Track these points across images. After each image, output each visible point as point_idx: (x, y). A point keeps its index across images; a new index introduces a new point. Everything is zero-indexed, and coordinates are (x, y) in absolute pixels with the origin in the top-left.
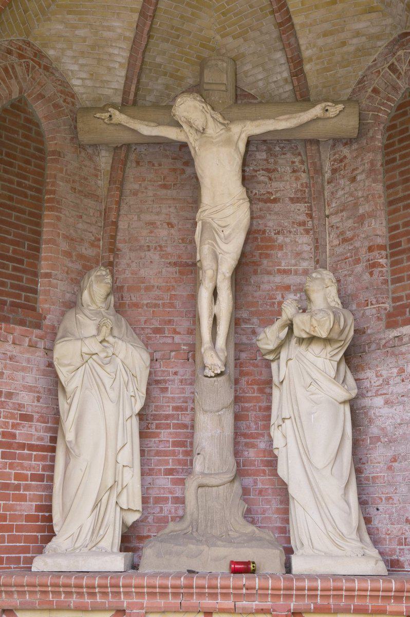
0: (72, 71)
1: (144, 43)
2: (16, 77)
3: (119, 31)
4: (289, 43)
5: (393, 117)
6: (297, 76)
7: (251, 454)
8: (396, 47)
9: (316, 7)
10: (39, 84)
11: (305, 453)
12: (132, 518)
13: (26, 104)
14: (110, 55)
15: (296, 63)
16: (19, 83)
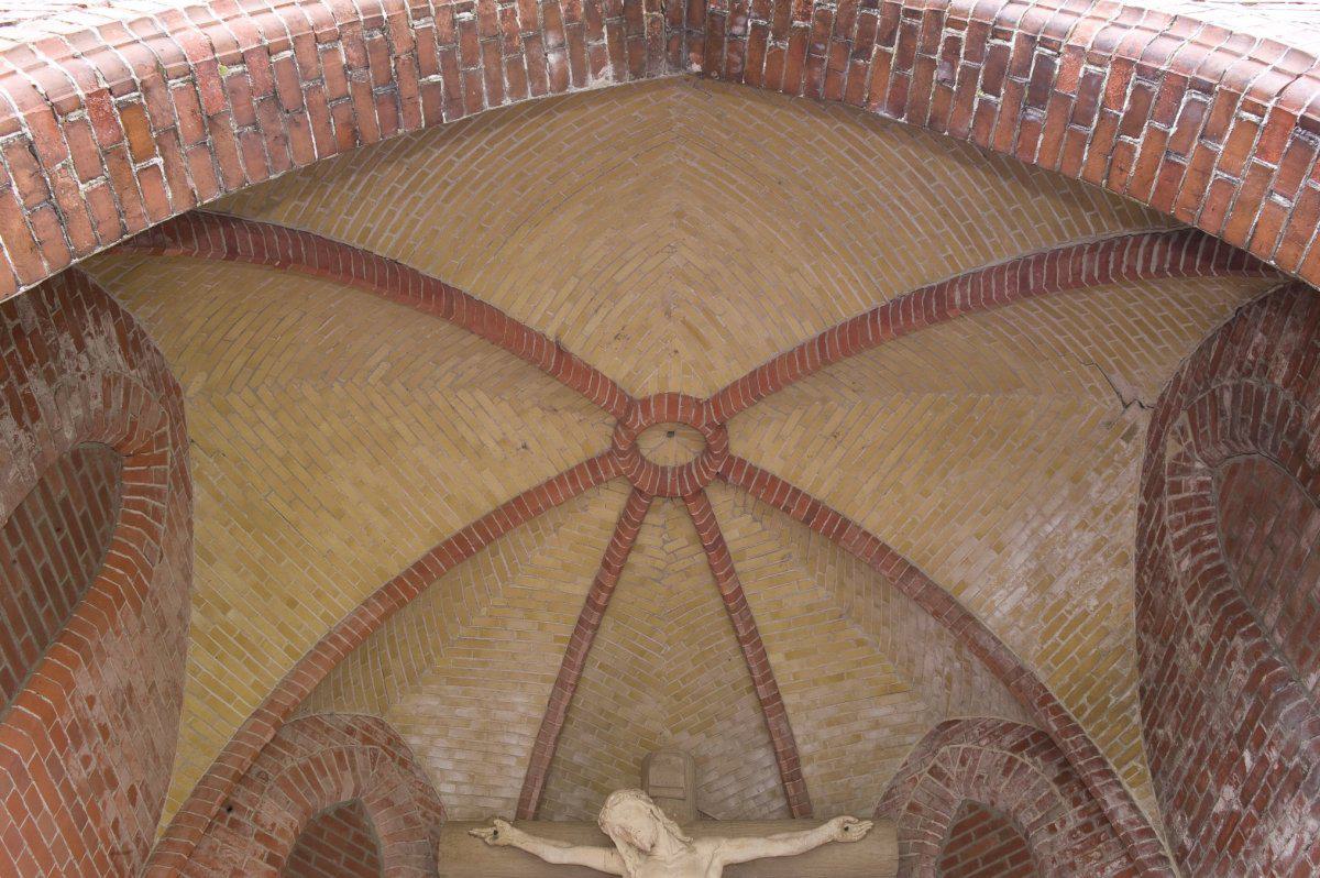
0: (442, 770)
1: (558, 725)
2: (354, 769)
3: (522, 709)
4: (779, 730)
5: (947, 847)
6: (792, 780)
8: (936, 743)
9: (815, 683)
10: (387, 783)
13: (361, 812)
14: (504, 745)
15: (789, 764)
16: (356, 778)
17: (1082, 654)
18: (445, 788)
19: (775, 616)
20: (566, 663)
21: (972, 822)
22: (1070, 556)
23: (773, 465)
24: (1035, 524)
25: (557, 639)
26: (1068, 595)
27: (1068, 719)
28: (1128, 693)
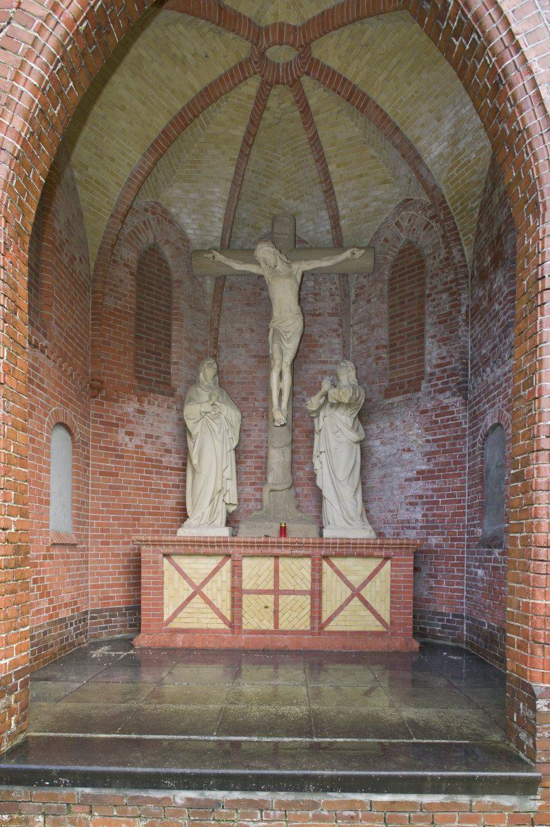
0: (187, 223)
2: (152, 228)
7: (300, 474)
10: (166, 233)
11: (333, 472)
12: (232, 509)
14: (212, 212)
16: (153, 232)
17: (463, 181)
18: (189, 231)
19: (333, 144)
20: (236, 173)
21: (409, 249)
22: (469, 129)
23: (333, 62)
24: (458, 108)
25: (231, 159)
26: (464, 149)
27: (450, 212)
28: (477, 203)
